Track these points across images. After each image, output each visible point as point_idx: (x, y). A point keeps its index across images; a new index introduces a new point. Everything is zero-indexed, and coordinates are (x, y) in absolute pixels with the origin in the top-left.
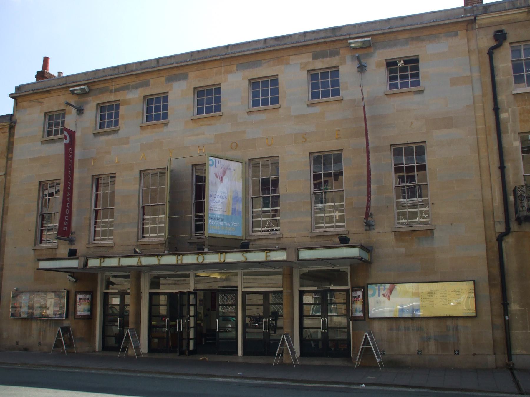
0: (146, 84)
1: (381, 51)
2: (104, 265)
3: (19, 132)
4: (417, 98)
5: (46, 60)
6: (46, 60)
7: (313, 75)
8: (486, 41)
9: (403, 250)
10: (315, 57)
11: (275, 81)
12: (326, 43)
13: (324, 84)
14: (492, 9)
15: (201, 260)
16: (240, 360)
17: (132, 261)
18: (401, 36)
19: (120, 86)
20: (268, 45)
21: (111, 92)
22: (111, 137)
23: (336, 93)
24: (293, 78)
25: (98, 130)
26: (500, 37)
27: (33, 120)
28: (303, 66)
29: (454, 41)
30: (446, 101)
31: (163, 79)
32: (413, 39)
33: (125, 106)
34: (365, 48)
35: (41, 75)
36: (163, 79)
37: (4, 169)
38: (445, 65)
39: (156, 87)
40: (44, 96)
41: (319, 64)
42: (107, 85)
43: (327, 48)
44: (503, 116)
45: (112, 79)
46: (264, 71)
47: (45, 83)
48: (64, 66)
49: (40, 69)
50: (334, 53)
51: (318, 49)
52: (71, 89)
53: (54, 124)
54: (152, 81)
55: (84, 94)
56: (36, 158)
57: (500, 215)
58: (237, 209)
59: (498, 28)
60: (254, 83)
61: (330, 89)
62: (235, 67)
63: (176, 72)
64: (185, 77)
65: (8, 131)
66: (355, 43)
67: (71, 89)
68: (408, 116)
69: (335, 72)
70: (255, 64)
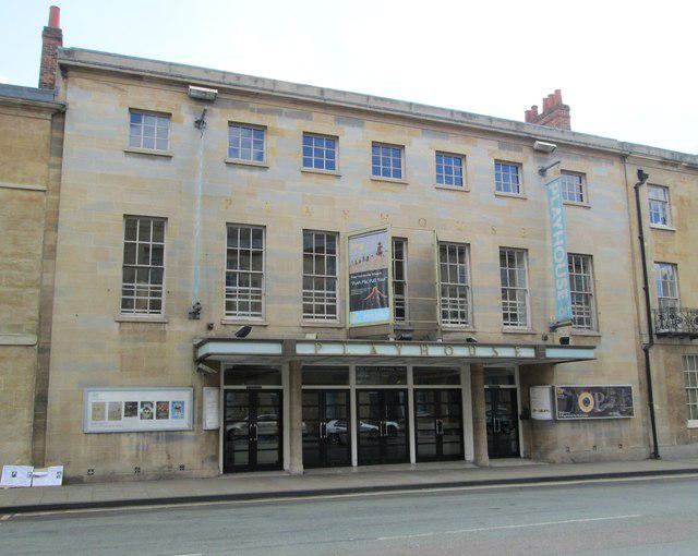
6: (55, 12)
39: (323, 124)
57: (645, 330)
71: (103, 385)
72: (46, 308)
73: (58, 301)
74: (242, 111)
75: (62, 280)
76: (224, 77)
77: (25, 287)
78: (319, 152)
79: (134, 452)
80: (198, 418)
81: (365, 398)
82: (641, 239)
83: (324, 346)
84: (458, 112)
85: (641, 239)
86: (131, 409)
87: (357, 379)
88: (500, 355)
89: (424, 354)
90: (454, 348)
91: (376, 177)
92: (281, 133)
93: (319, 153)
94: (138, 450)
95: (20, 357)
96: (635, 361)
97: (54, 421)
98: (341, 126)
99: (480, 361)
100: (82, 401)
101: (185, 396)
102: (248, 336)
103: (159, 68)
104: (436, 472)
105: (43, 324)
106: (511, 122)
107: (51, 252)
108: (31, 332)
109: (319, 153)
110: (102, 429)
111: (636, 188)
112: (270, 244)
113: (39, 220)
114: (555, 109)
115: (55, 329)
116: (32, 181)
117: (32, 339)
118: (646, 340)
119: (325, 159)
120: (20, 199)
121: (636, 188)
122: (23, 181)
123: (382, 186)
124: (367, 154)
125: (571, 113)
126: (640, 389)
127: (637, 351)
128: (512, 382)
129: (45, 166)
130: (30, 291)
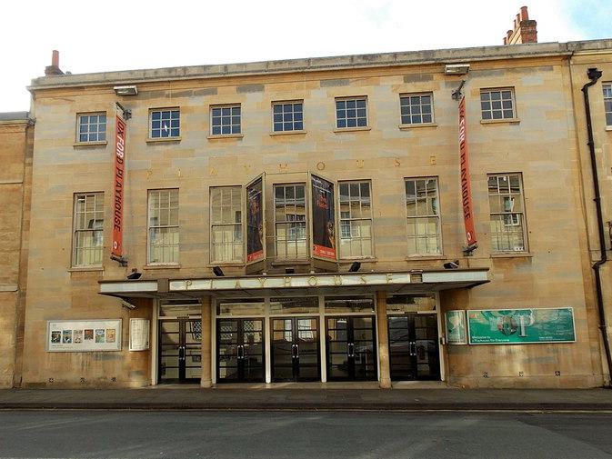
0: (213, 92)
1: (476, 79)
2: (190, 288)
3: (39, 133)
4: (512, 128)
5: (56, 55)
6: (56, 55)
7: (404, 98)
8: (581, 78)
9: (502, 276)
10: (408, 79)
11: (362, 101)
12: (409, 66)
13: (415, 109)
14: (585, 47)
15: (338, 283)
16: (325, 387)
17: (205, 285)
18: (496, 66)
19: (177, 91)
20: (355, 63)
21: (168, 96)
22: (170, 147)
23: (427, 119)
24: (383, 97)
25: (212, 136)
26: (594, 75)
27: (59, 121)
28: (395, 88)
29: (549, 75)
30: (542, 137)
31: (234, 88)
32: (508, 70)
33: (186, 115)
34: (459, 75)
35: (53, 70)
36: (234, 88)
37: (22, 176)
38: (546, 102)
39: (227, 95)
40: (76, 93)
41: (412, 88)
42: (163, 88)
43: (420, 72)
44: (597, 151)
45: (169, 81)
46: (352, 90)
47: (55, 80)
48: (75, 65)
49: (50, 64)
50: (427, 78)
51: (410, 72)
52: (115, 88)
53: (89, 130)
54: (219, 89)
55: (132, 95)
56: (62, 165)
57: (595, 245)
58: (502, 222)
59: (592, 67)
60: (340, 102)
61: (231, 116)
62: (319, 83)
63: (248, 82)
64: (261, 88)
65: (24, 130)
66: (450, 68)
67: (115, 88)
68: (497, 148)
69: (428, 95)
70: (342, 82)
71: (61, 317)
72: (23, 266)
73: (31, 260)
74: (159, 99)
75: (33, 244)
76: (145, 74)
77: (10, 252)
78: (226, 120)
79: (81, 367)
80: (125, 342)
81: (331, 324)
82: (591, 145)
83: (396, 276)
84: (359, 56)
85: (591, 145)
86: (89, 334)
87: (326, 305)
88: (368, 283)
89: (287, 285)
90: (209, 288)
91: (487, 121)
92: (191, 110)
93: (226, 121)
94: (83, 365)
95: (7, 300)
96: (580, 280)
97: (28, 342)
98: (243, 94)
99: (456, 286)
100: (45, 329)
101: (114, 325)
102: (350, 266)
103: (96, 78)
104: (408, 385)
105: (21, 277)
106: (418, 53)
107: (25, 226)
108: (14, 282)
109: (497, 105)
110: (59, 349)
111: (585, 90)
112: (184, 201)
113: (18, 204)
114: (527, 26)
115: (30, 279)
116: (14, 178)
117: (14, 288)
118: (597, 257)
119: (346, 119)
120: (7, 190)
121: (585, 90)
122: (9, 178)
123: (281, 138)
124: (269, 113)
125: (538, 28)
126: (588, 311)
127: (583, 269)
128: (434, 309)
129: (22, 165)
130: (14, 254)
